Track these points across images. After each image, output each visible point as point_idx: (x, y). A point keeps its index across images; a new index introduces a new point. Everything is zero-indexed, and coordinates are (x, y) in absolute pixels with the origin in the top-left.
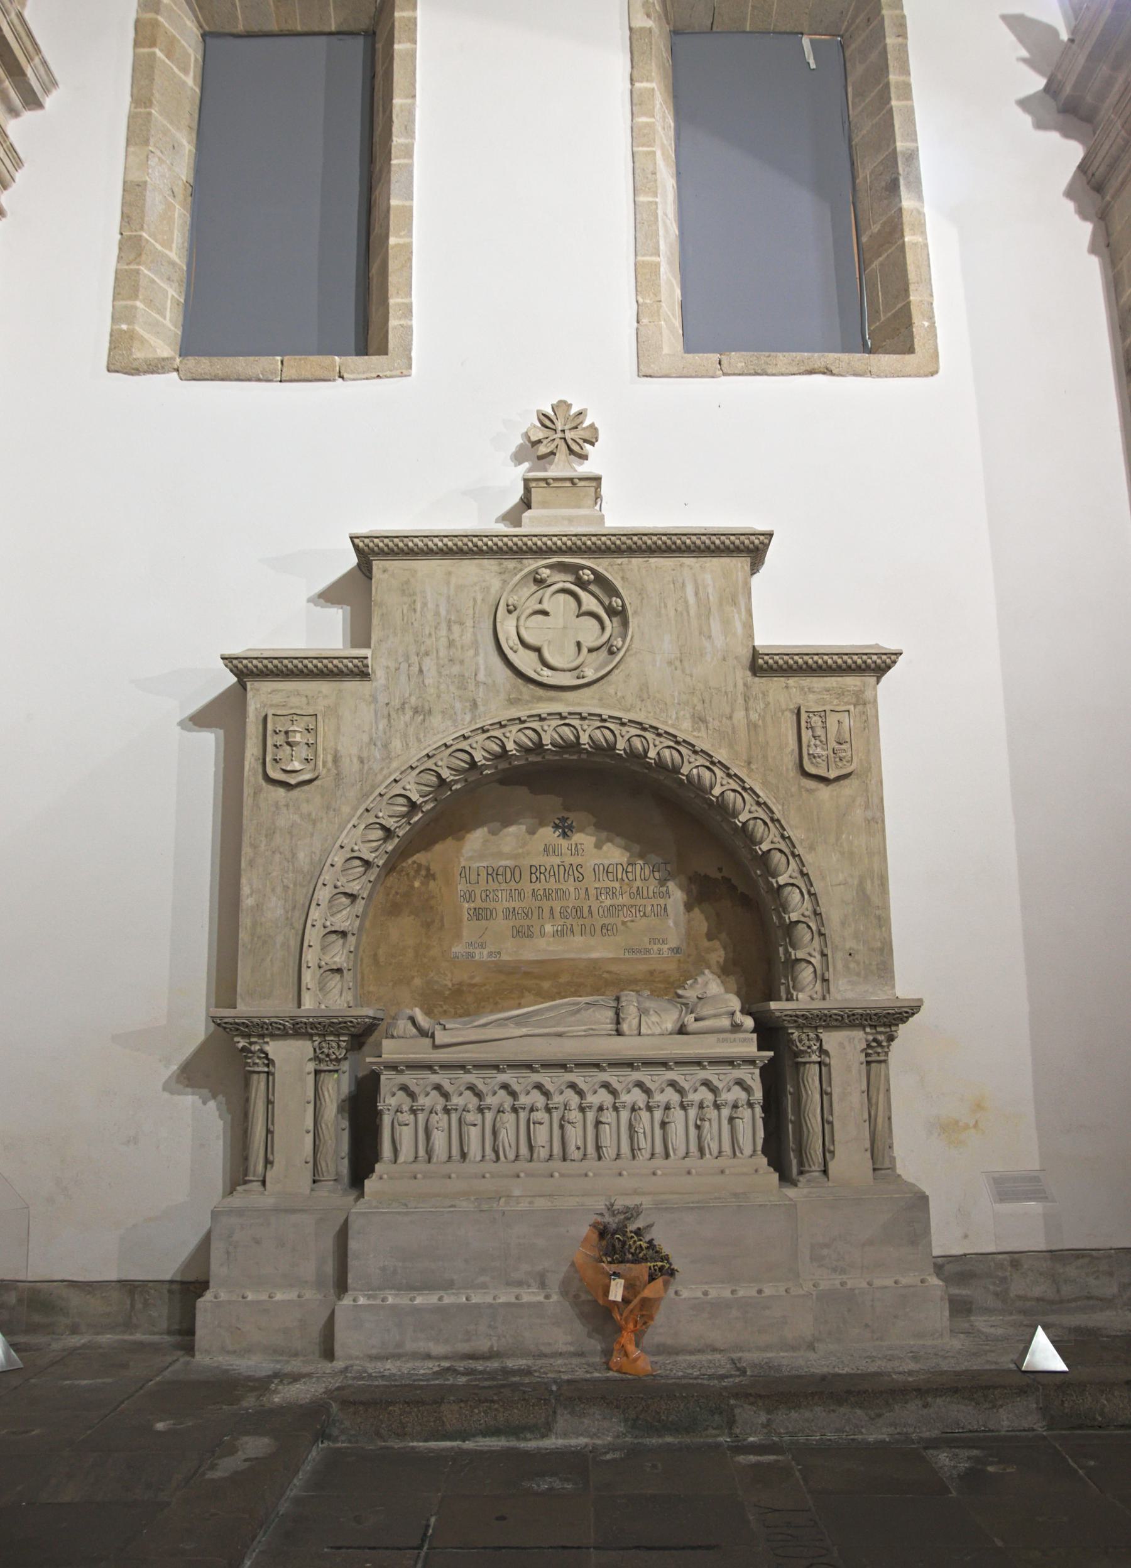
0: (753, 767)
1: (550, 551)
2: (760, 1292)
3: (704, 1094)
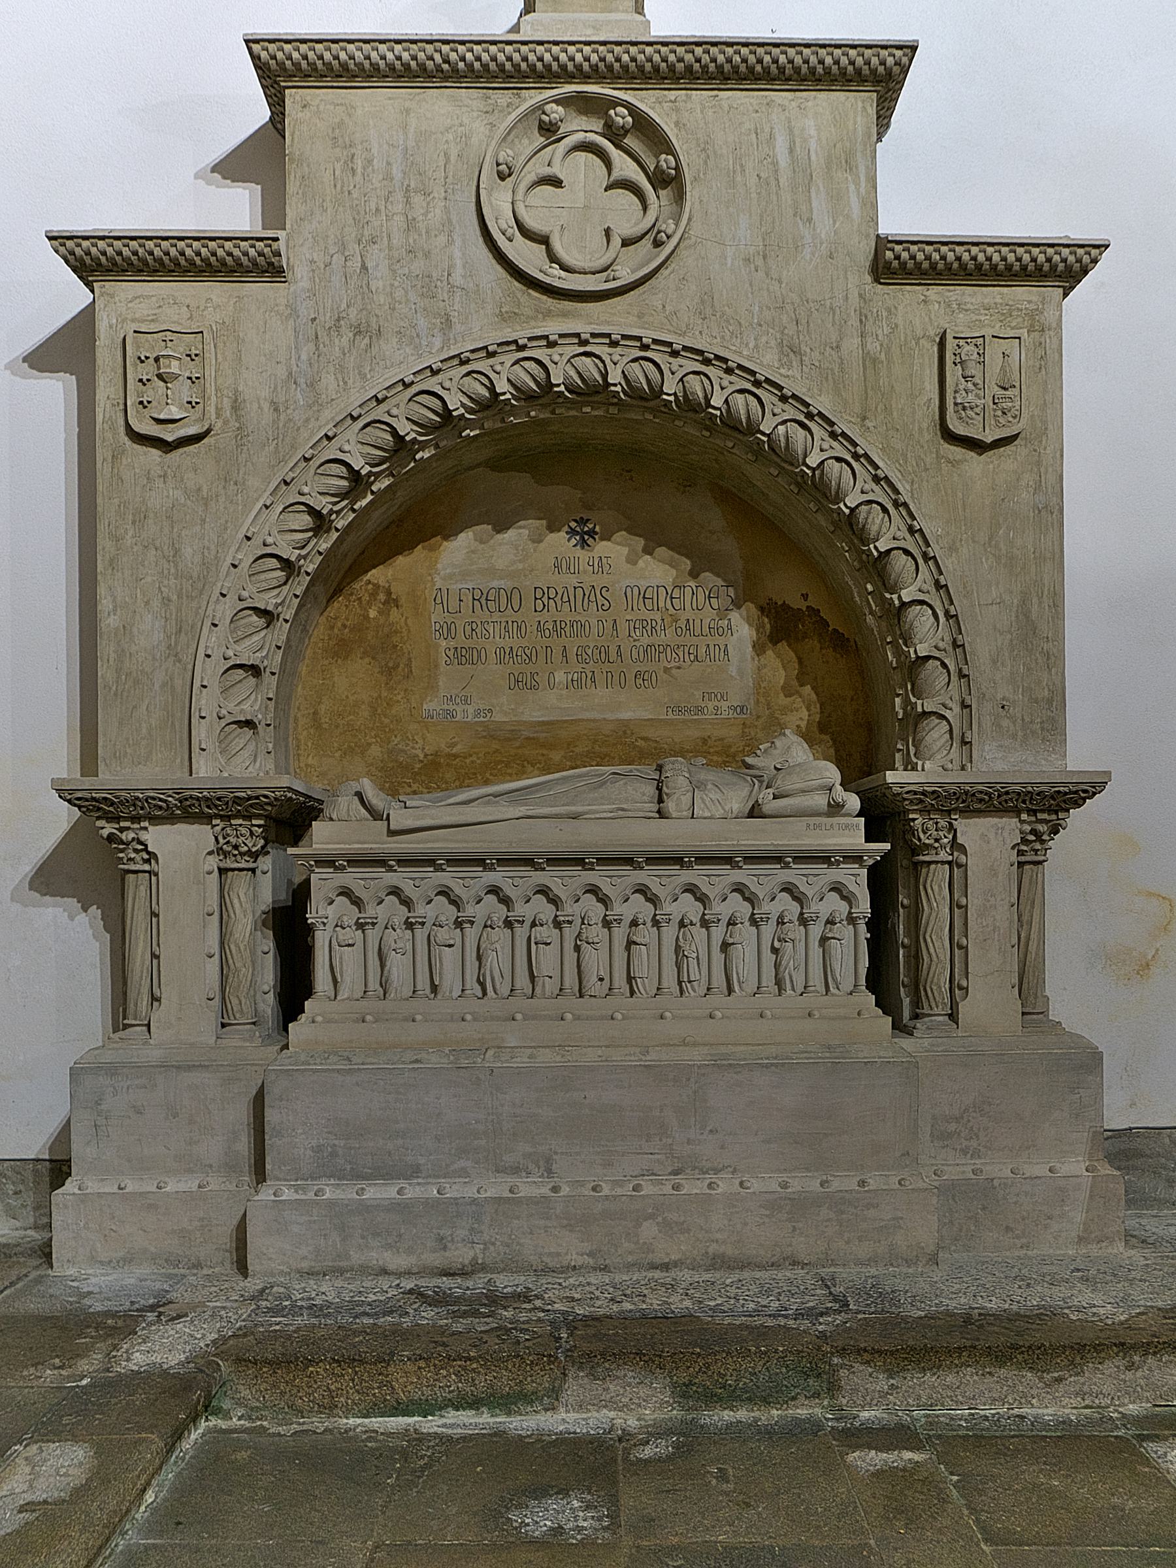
0: (869, 424)
1: (564, 75)
2: (862, 1183)
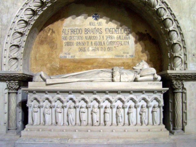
3: (143, 103)
